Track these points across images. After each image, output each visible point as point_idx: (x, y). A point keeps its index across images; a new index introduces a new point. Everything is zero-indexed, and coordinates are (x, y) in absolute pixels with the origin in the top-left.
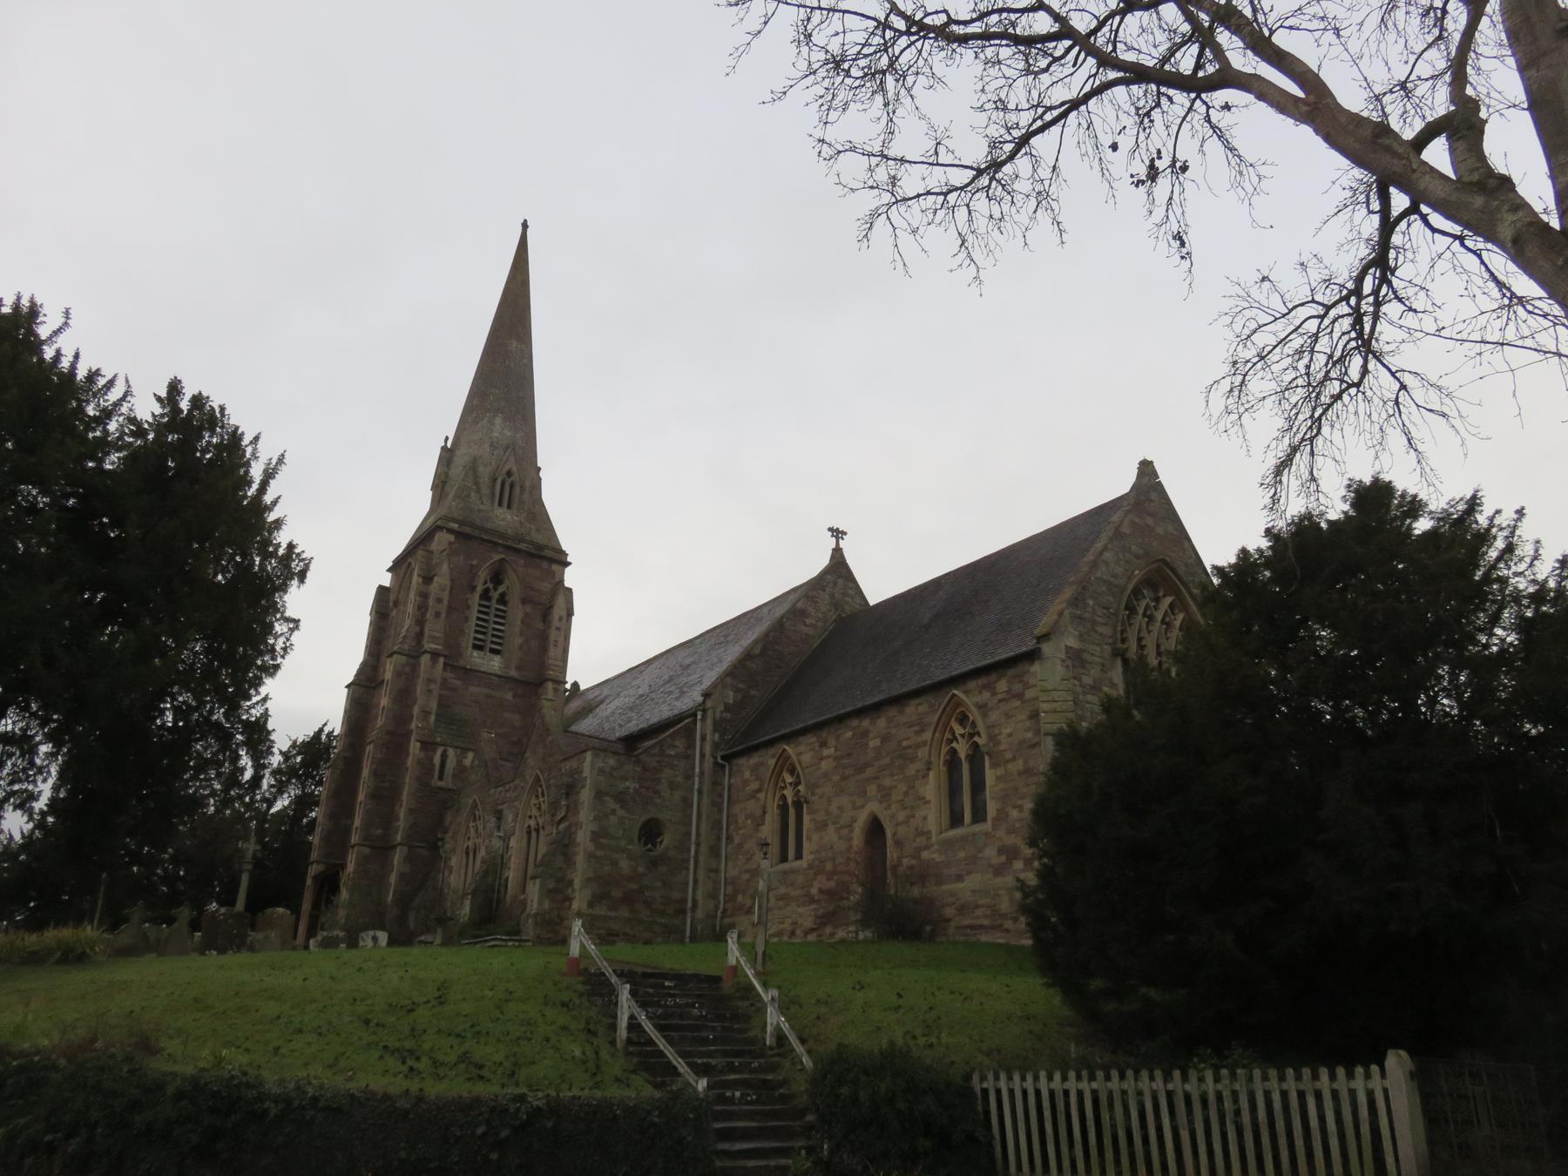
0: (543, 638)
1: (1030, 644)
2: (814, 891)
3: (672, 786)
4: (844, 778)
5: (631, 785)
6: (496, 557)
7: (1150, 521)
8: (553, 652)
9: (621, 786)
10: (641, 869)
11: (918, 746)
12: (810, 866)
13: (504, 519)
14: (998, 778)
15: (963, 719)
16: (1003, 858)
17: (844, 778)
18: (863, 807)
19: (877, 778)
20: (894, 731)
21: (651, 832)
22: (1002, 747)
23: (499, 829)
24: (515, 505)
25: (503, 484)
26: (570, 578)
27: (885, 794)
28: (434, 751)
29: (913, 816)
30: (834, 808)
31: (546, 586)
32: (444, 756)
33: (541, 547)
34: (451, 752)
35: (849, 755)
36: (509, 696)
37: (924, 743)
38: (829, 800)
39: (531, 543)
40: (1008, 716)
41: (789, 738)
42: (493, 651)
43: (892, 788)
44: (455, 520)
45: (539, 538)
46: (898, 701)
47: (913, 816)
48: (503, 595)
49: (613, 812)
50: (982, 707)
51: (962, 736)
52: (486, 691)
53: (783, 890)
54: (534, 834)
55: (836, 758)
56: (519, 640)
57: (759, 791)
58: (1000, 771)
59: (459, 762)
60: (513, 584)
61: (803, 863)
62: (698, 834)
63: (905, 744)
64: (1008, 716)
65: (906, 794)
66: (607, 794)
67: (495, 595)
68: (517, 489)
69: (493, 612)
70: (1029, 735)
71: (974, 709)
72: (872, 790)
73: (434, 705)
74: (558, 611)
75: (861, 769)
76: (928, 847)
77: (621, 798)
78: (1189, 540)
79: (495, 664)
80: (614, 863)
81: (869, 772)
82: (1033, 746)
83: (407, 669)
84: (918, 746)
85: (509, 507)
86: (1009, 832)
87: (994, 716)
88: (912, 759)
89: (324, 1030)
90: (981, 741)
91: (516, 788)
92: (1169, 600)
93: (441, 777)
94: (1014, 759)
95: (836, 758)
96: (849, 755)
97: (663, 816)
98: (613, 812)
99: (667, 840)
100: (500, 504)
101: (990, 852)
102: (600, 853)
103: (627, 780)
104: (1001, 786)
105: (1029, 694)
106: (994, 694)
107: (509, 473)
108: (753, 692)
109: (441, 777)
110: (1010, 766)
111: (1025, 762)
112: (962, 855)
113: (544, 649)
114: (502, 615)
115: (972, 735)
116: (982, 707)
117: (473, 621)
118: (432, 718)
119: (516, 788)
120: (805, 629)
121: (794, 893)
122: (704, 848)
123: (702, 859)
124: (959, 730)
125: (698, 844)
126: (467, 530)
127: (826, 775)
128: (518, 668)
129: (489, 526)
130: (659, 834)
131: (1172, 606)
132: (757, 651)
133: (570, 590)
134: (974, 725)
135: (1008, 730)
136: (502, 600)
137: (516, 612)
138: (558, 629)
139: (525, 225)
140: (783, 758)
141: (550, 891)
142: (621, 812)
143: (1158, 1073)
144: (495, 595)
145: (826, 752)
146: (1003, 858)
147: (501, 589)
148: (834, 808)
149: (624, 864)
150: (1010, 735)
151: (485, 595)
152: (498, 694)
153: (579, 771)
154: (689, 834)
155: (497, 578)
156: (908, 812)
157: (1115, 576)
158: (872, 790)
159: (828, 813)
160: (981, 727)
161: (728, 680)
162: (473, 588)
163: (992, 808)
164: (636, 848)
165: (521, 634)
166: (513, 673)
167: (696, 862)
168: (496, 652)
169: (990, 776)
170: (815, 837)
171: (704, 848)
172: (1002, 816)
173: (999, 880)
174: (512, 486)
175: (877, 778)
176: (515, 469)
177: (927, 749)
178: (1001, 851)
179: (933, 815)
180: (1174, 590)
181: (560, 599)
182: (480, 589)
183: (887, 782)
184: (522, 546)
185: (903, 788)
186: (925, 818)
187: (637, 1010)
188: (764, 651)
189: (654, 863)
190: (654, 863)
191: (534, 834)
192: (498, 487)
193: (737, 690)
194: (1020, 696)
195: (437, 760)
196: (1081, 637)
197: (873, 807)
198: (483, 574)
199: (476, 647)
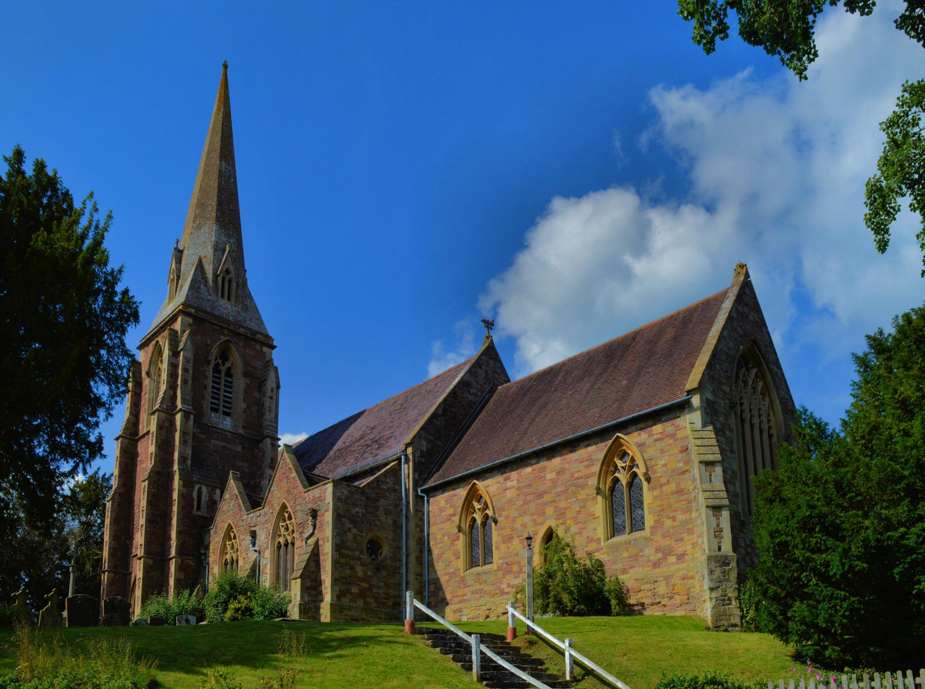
0: (260, 405)
1: (684, 398)
2: (504, 586)
3: (387, 512)
4: (526, 503)
5: (359, 510)
6: (224, 339)
7: (746, 310)
8: (268, 416)
9: (353, 511)
10: (369, 573)
11: (587, 477)
12: (499, 569)
13: (227, 308)
14: (655, 498)
15: (623, 455)
16: (660, 555)
17: (526, 503)
18: (542, 523)
19: (554, 501)
20: (567, 466)
21: (374, 547)
22: (658, 475)
23: (254, 545)
24: (233, 298)
25: (223, 279)
26: (277, 357)
27: (561, 514)
28: (193, 487)
29: (586, 528)
30: (517, 525)
31: (259, 364)
32: (200, 492)
33: (255, 333)
34: (204, 489)
35: (529, 486)
36: (239, 449)
37: (593, 474)
38: (514, 520)
39: (247, 328)
40: (662, 451)
41: (482, 474)
42: (225, 413)
43: (566, 509)
44: (193, 307)
45: (253, 325)
46: (571, 445)
47: (586, 528)
48: (229, 369)
49: (349, 529)
50: (640, 445)
51: (479, 509)
52: (224, 444)
53: (477, 587)
54: (283, 548)
55: (518, 489)
56: (243, 406)
57: (453, 515)
58: (657, 492)
59: (211, 497)
60: (236, 360)
61: (494, 566)
62: (407, 548)
63: (576, 475)
64: (662, 451)
65: (579, 512)
66: (344, 516)
67: (223, 369)
68: (234, 285)
69: (223, 382)
70: (681, 464)
71: (635, 448)
72: (550, 510)
73: (189, 452)
74: (270, 384)
75: (540, 496)
76: (597, 550)
77: (353, 520)
78: (766, 327)
79: (227, 424)
80: (352, 568)
81: (547, 498)
82: (684, 472)
83: (167, 424)
84: (587, 477)
85: (229, 299)
86: (664, 536)
87: (650, 452)
88: (583, 487)
89: (519, 596)
90: (490, 512)
91: (266, 514)
92: (754, 371)
93: (199, 508)
94: (668, 482)
95: (518, 489)
96: (529, 486)
97: (381, 534)
98: (349, 529)
99: (386, 550)
100: (222, 297)
101: (650, 552)
102: (342, 560)
103: (357, 506)
104: (658, 503)
105: (680, 434)
106: (651, 435)
107: (227, 272)
108: (438, 443)
109: (199, 508)
110: (664, 488)
111: (678, 484)
112: (626, 554)
113: (261, 414)
114: (229, 385)
115: (484, 509)
116: (640, 445)
117: (210, 390)
118: (189, 462)
119: (266, 514)
120: (471, 397)
121: (487, 588)
122: (412, 559)
123: (411, 566)
124: (620, 464)
125: (407, 556)
126: (202, 315)
127: (510, 501)
128: (244, 427)
129: (216, 313)
130: (380, 548)
131: (756, 376)
132: (440, 412)
133: (276, 368)
134: (633, 460)
135: (663, 462)
136: (229, 374)
137: (240, 383)
138: (271, 398)
139: (226, 66)
140: (474, 489)
141: (308, 588)
142: (354, 531)
143: (909, 673)
144: (223, 369)
145: (509, 484)
146: (660, 555)
147: (228, 365)
148: (517, 525)
149: (359, 569)
150: (665, 465)
151: (216, 370)
152: (232, 447)
153: (321, 499)
154: (400, 548)
155: (224, 355)
156: (580, 525)
157: (730, 349)
158: (550, 510)
159: (513, 529)
160: (639, 461)
161: (423, 432)
162: (209, 362)
163: (649, 520)
164: (365, 557)
165: (244, 401)
166: (241, 431)
167: (407, 568)
168: (228, 414)
169: (648, 496)
170: (503, 547)
171: (412, 559)
172: (658, 524)
173: (657, 571)
174: (230, 282)
175: (554, 501)
176: (231, 268)
177: (596, 478)
178: (658, 550)
179: (600, 528)
180: (759, 366)
181: (272, 374)
182: (213, 363)
183: (562, 504)
184: (242, 330)
185: (576, 507)
186: (595, 529)
187: (483, 648)
188: (445, 410)
189: (378, 569)
190: (378, 569)
191: (283, 548)
192: (220, 282)
193: (429, 441)
194: (673, 436)
195: (195, 495)
196: (714, 393)
197: (552, 523)
198: (214, 351)
199: (213, 409)
